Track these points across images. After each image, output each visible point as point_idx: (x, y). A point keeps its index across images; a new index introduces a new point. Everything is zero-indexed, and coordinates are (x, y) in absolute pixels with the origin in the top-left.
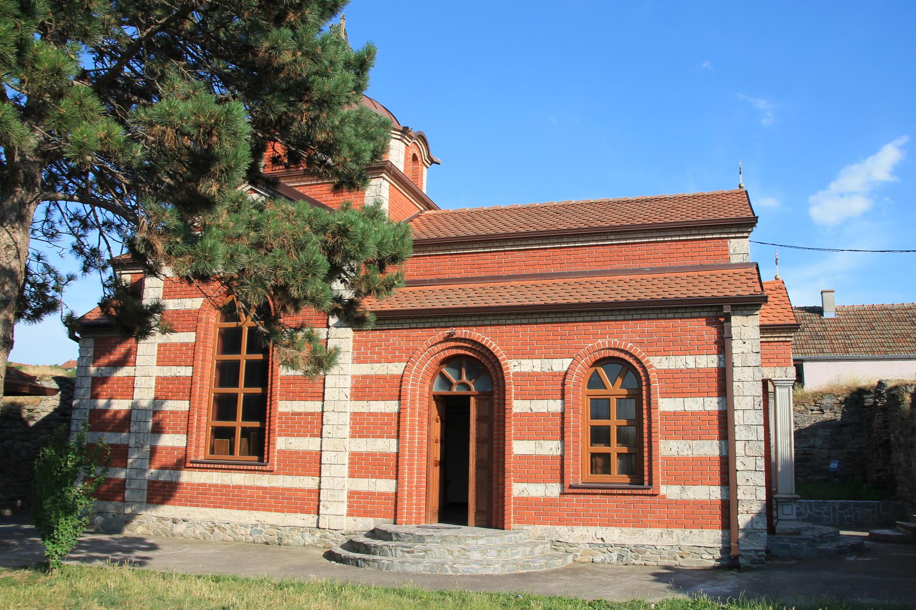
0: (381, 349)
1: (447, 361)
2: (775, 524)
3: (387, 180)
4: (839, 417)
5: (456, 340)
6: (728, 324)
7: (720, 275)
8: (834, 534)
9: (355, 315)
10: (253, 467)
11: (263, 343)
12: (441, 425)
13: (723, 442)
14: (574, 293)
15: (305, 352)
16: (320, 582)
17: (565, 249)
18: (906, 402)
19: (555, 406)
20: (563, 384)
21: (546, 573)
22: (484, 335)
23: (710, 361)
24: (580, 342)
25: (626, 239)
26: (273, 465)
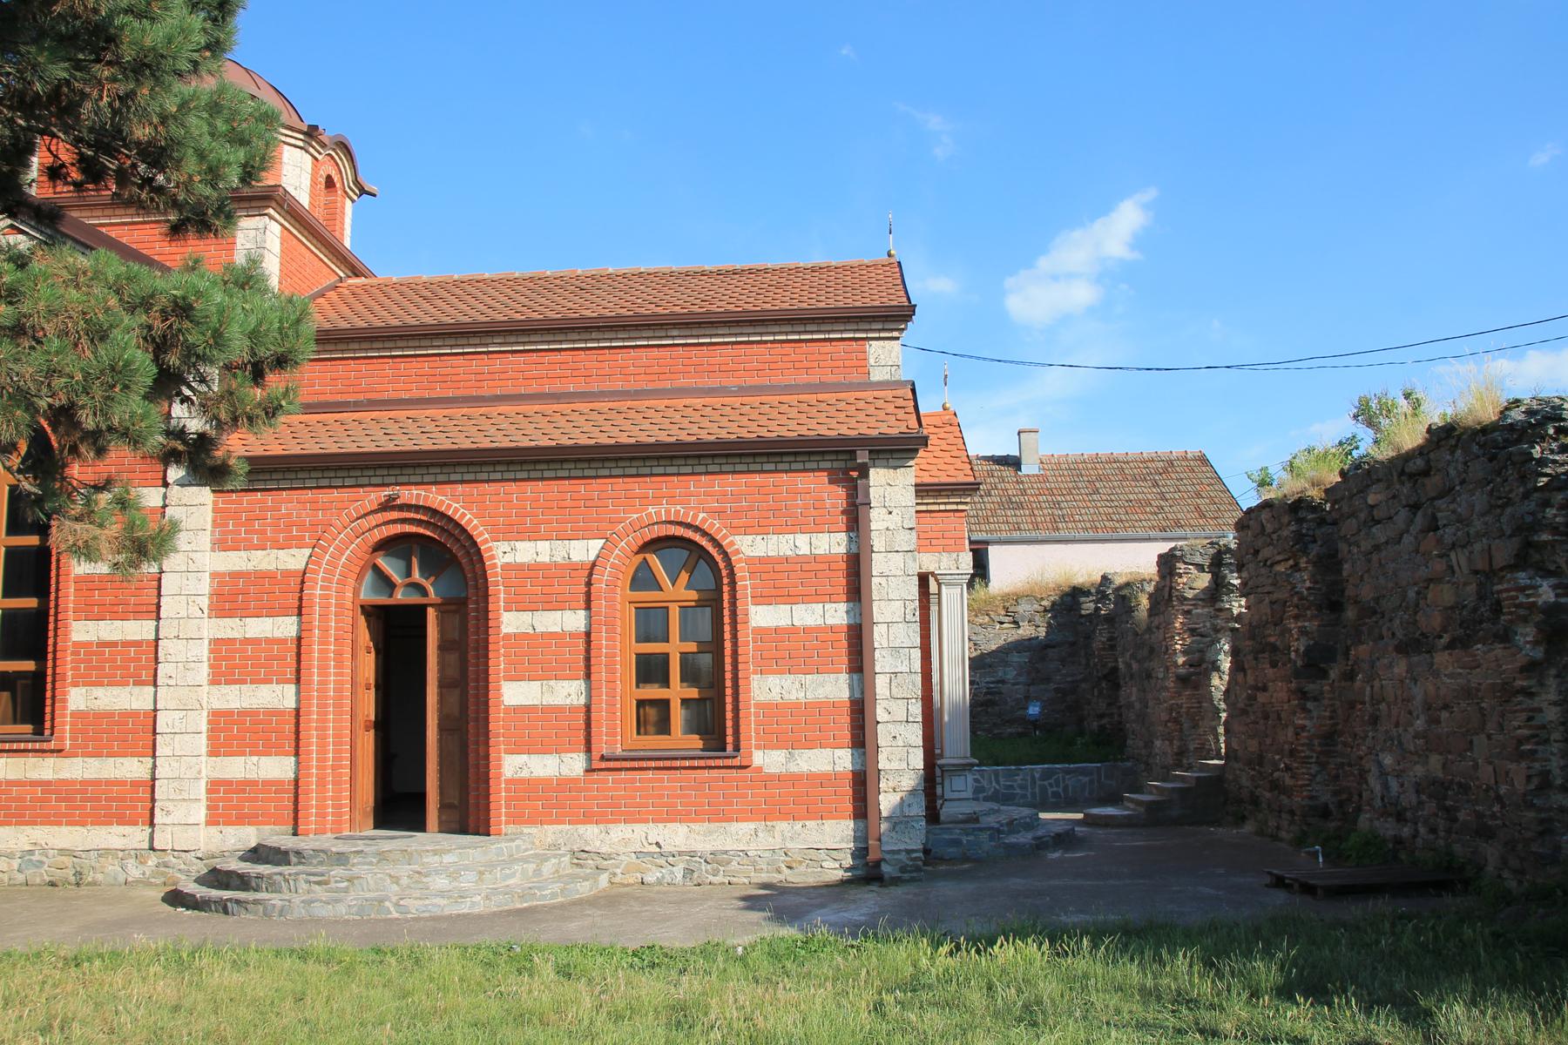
0: (264, 525)
1: (385, 546)
2: (938, 807)
3: (276, 221)
4: (1042, 632)
5: (402, 508)
6: (864, 481)
7: (852, 400)
8: (1031, 818)
9: (209, 462)
10: (22, 746)
11: (30, 513)
12: (377, 658)
13: (855, 676)
14: (607, 426)
15: (114, 529)
16: (153, 947)
17: (594, 352)
18: (1142, 607)
19: (575, 621)
20: (589, 584)
21: (562, 906)
22: (451, 500)
23: (834, 544)
24: (617, 512)
25: (698, 337)
26: (62, 739)
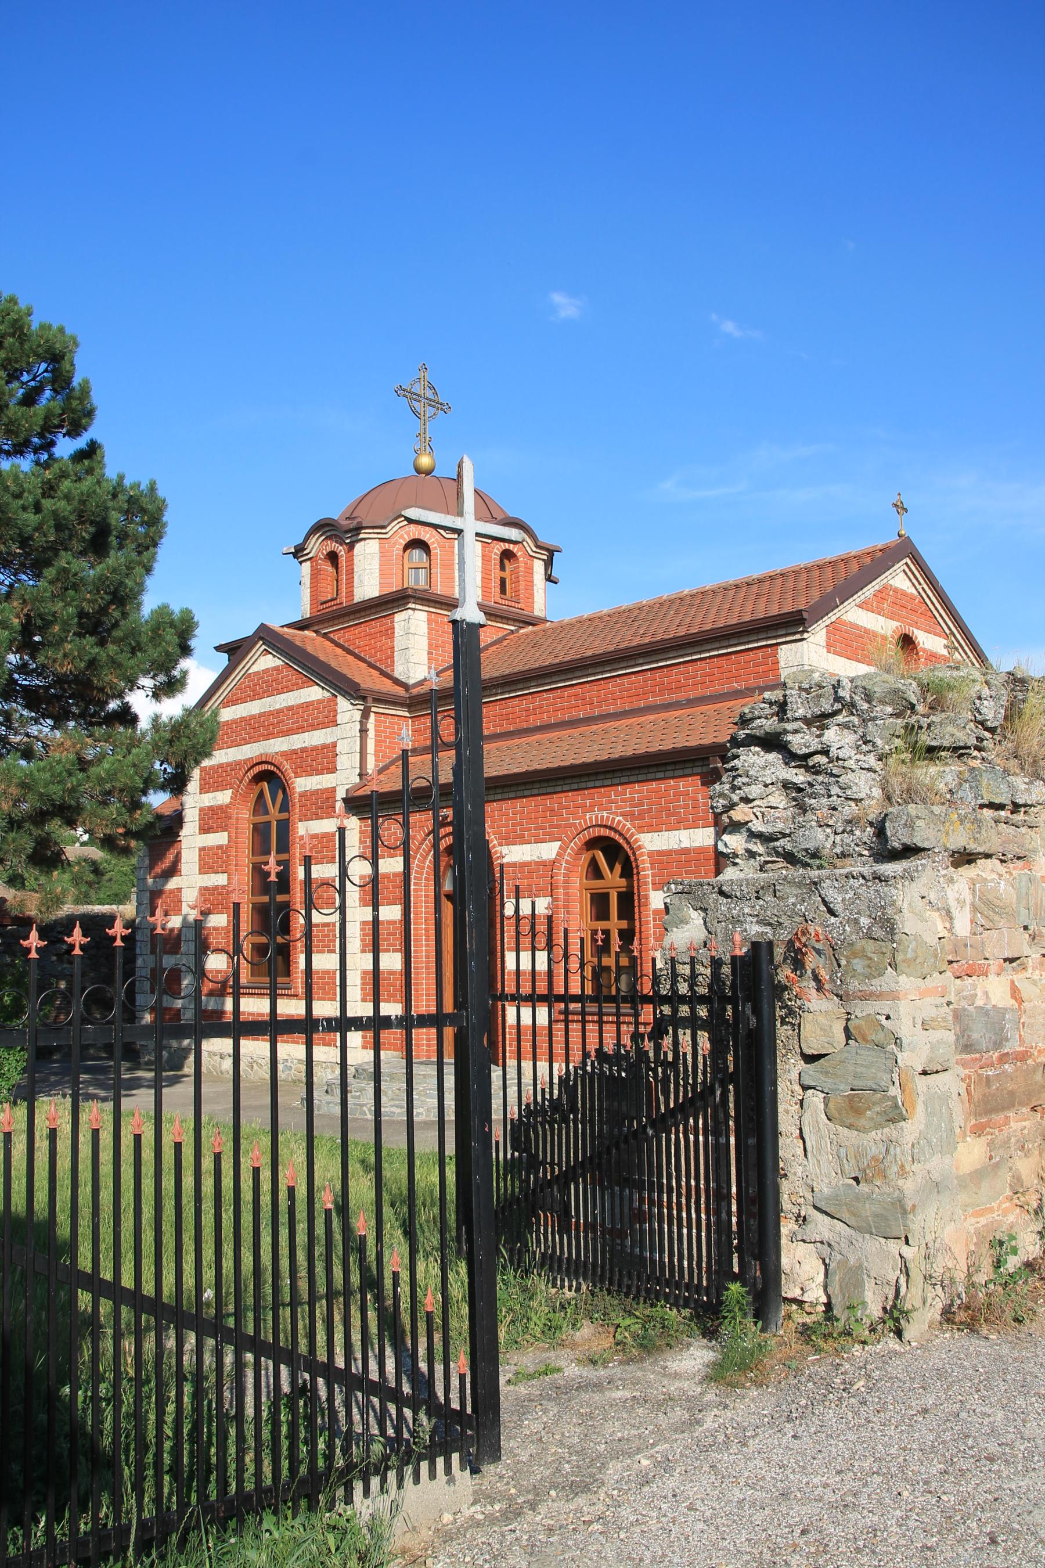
26: (296, 988)
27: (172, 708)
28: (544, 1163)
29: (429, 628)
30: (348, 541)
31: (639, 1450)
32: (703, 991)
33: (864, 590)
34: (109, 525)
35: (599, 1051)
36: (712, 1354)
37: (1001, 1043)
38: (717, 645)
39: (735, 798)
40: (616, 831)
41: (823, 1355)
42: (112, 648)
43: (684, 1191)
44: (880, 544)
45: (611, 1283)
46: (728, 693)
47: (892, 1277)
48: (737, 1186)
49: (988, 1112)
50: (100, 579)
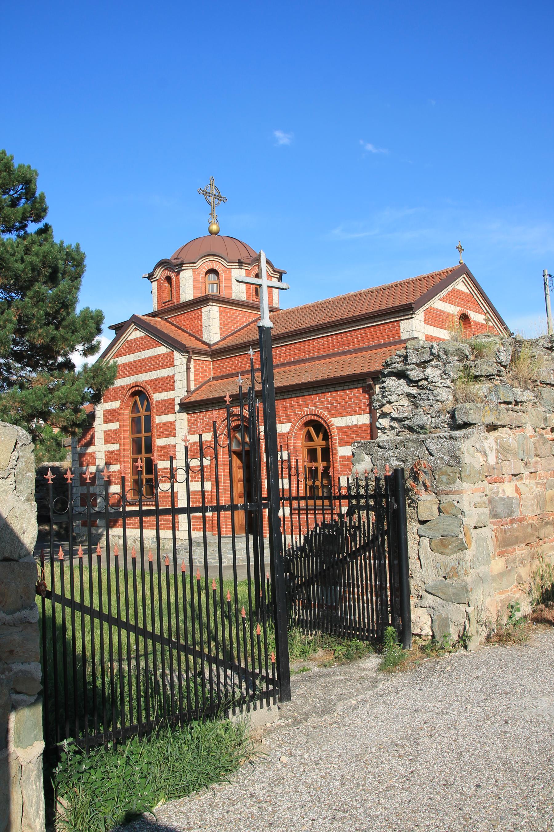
27: (92, 360)
28: (297, 576)
29: (220, 315)
30: (176, 271)
31: (350, 698)
32: (372, 492)
33: (443, 292)
34: (58, 267)
35: (323, 523)
36: (380, 660)
37: (511, 513)
38: (369, 321)
39: (384, 402)
40: (320, 417)
41: (431, 658)
42: (62, 331)
43: (364, 586)
44: (450, 267)
45: (331, 631)
46: (375, 346)
47: (462, 621)
48: (390, 583)
49: (505, 546)
50: (56, 296)
